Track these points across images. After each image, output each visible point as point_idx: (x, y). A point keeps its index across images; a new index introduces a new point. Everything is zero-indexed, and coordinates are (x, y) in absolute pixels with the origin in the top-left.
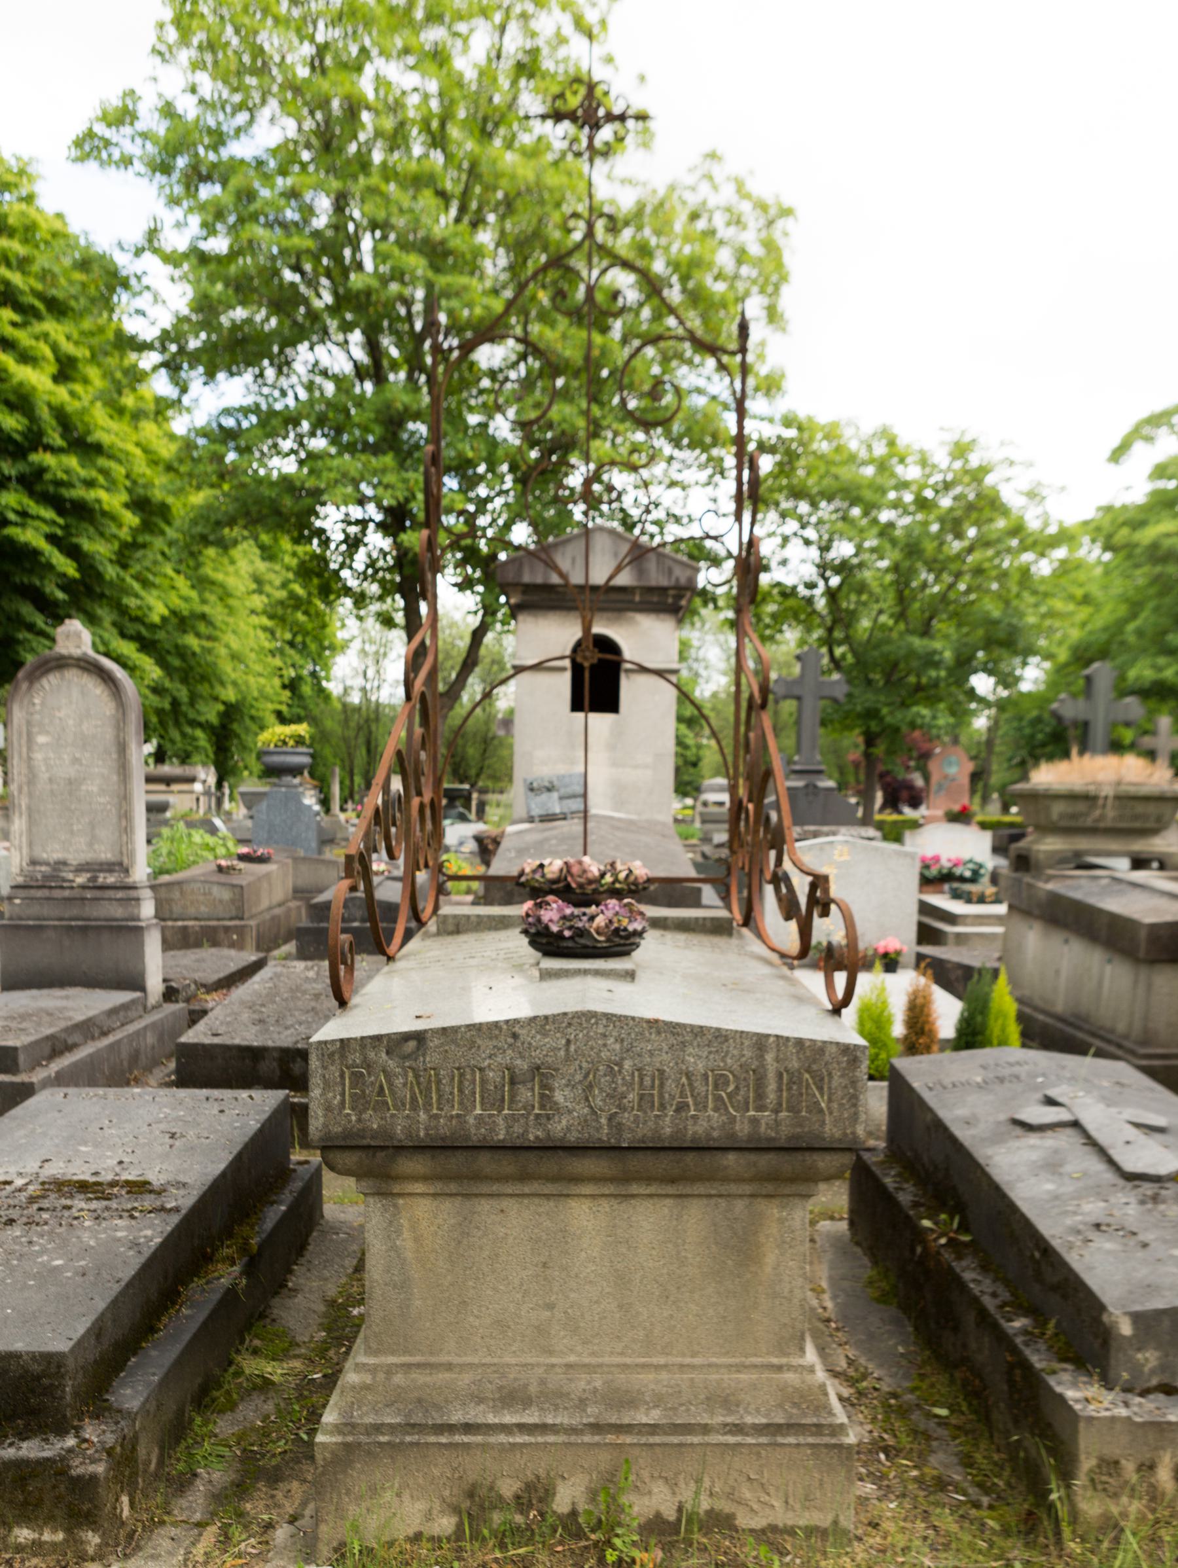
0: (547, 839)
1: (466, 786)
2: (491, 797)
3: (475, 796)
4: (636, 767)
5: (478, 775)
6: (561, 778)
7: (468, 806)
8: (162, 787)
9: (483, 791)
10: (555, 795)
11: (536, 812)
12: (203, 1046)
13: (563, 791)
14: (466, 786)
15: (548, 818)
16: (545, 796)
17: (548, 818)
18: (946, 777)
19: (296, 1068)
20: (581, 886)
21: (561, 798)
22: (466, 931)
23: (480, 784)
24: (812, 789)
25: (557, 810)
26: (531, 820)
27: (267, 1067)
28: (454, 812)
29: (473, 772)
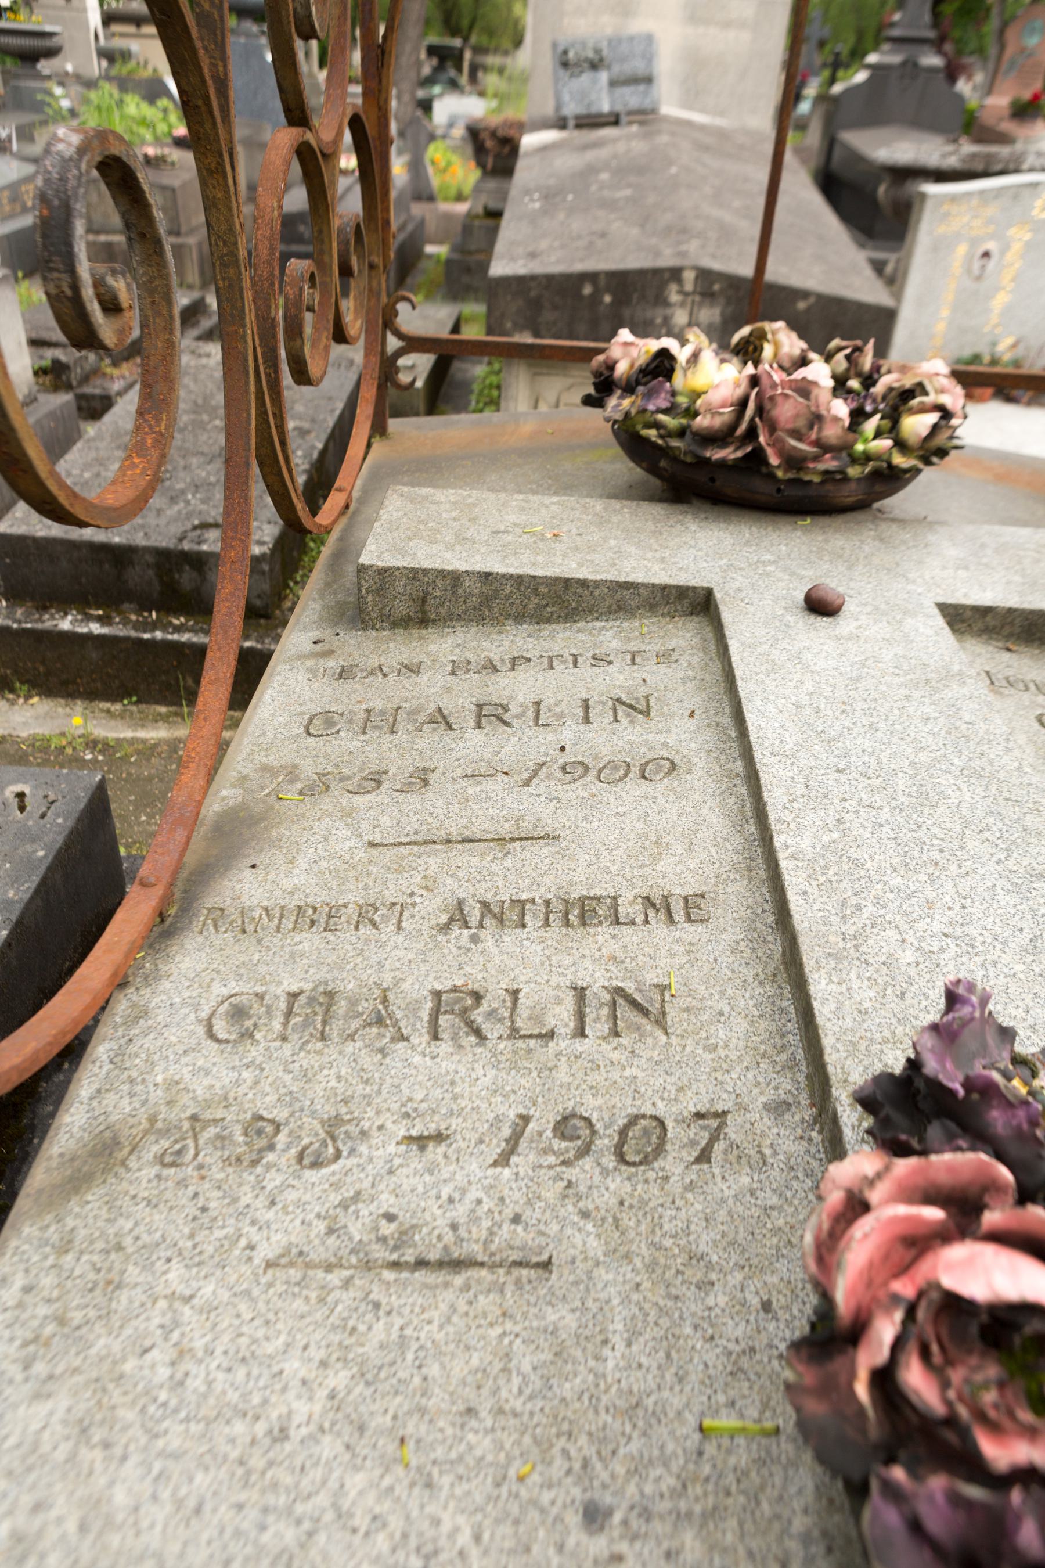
0: (591, 170)
1: (457, 42)
2: (491, 60)
3: (468, 55)
4: (727, 25)
5: (471, 28)
6: (614, 42)
7: (459, 69)
8: (131, 29)
9: (478, 50)
10: (604, 76)
11: (571, 109)
12: (35, 540)
13: (616, 69)
14: (457, 42)
15: (589, 122)
16: (586, 78)
17: (589, 122)
18: (1023, 50)
19: (186, 579)
20: (794, 462)
21: (613, 84)
22: (448, 620)
23: (474, 39)
24: (910, 66)
25: (606, 107)
26: (561, 124)
27: (138, 576)
28: (444, 77)
29: (465, 23)
